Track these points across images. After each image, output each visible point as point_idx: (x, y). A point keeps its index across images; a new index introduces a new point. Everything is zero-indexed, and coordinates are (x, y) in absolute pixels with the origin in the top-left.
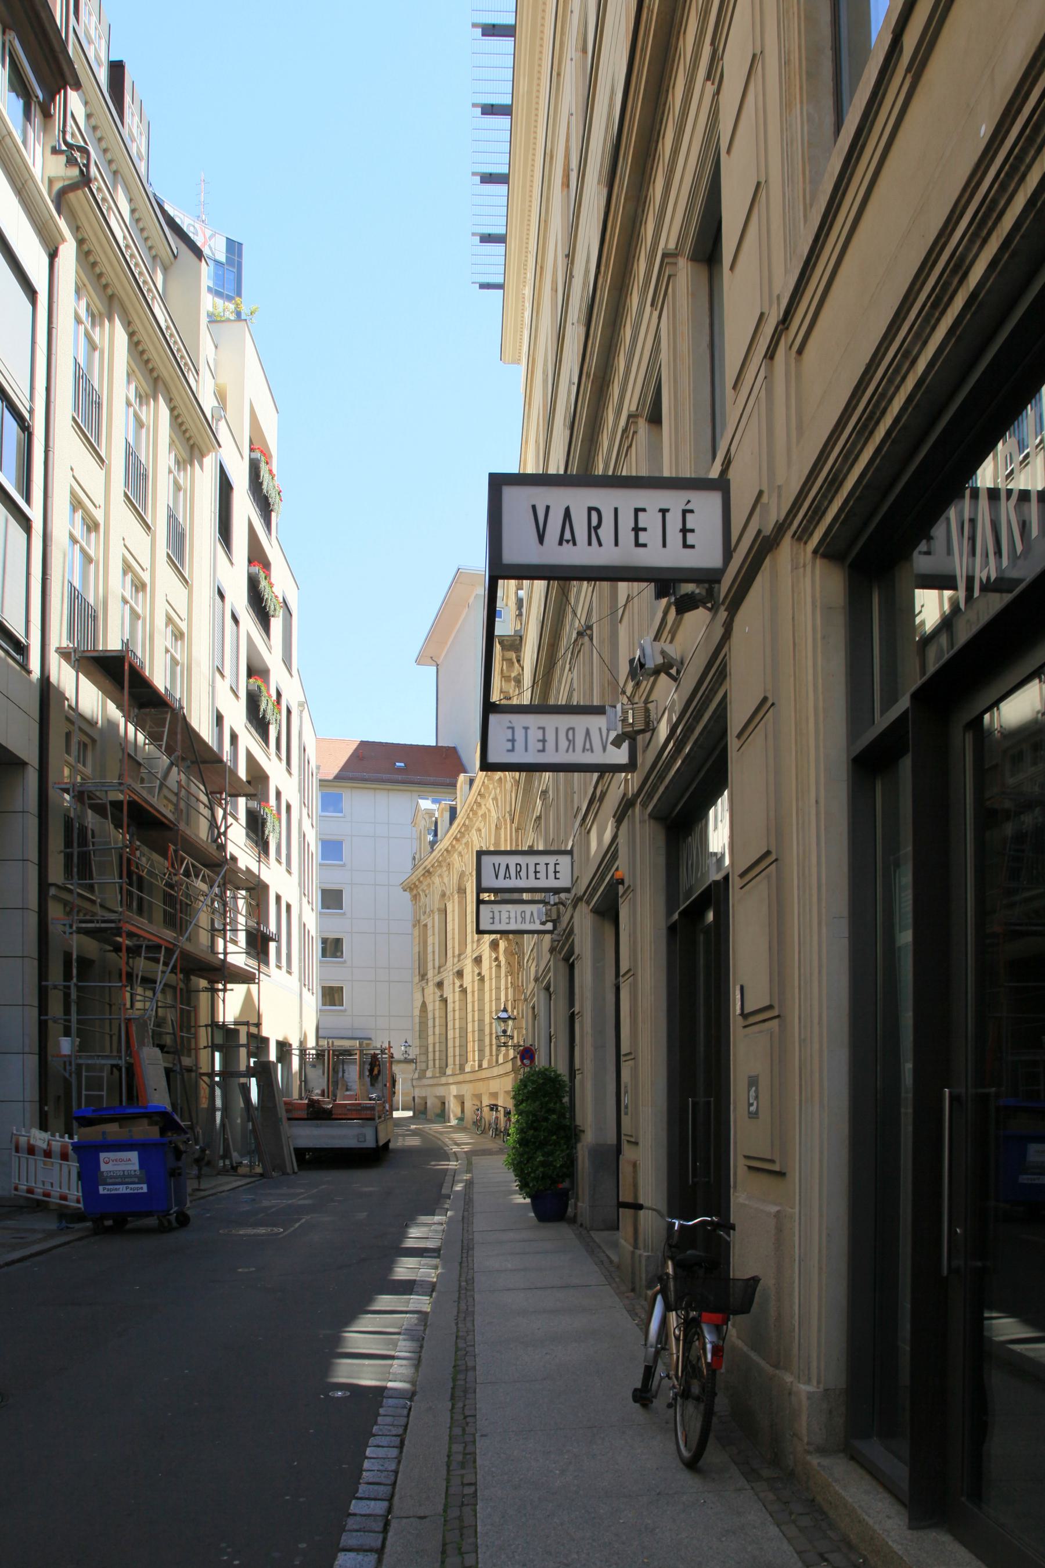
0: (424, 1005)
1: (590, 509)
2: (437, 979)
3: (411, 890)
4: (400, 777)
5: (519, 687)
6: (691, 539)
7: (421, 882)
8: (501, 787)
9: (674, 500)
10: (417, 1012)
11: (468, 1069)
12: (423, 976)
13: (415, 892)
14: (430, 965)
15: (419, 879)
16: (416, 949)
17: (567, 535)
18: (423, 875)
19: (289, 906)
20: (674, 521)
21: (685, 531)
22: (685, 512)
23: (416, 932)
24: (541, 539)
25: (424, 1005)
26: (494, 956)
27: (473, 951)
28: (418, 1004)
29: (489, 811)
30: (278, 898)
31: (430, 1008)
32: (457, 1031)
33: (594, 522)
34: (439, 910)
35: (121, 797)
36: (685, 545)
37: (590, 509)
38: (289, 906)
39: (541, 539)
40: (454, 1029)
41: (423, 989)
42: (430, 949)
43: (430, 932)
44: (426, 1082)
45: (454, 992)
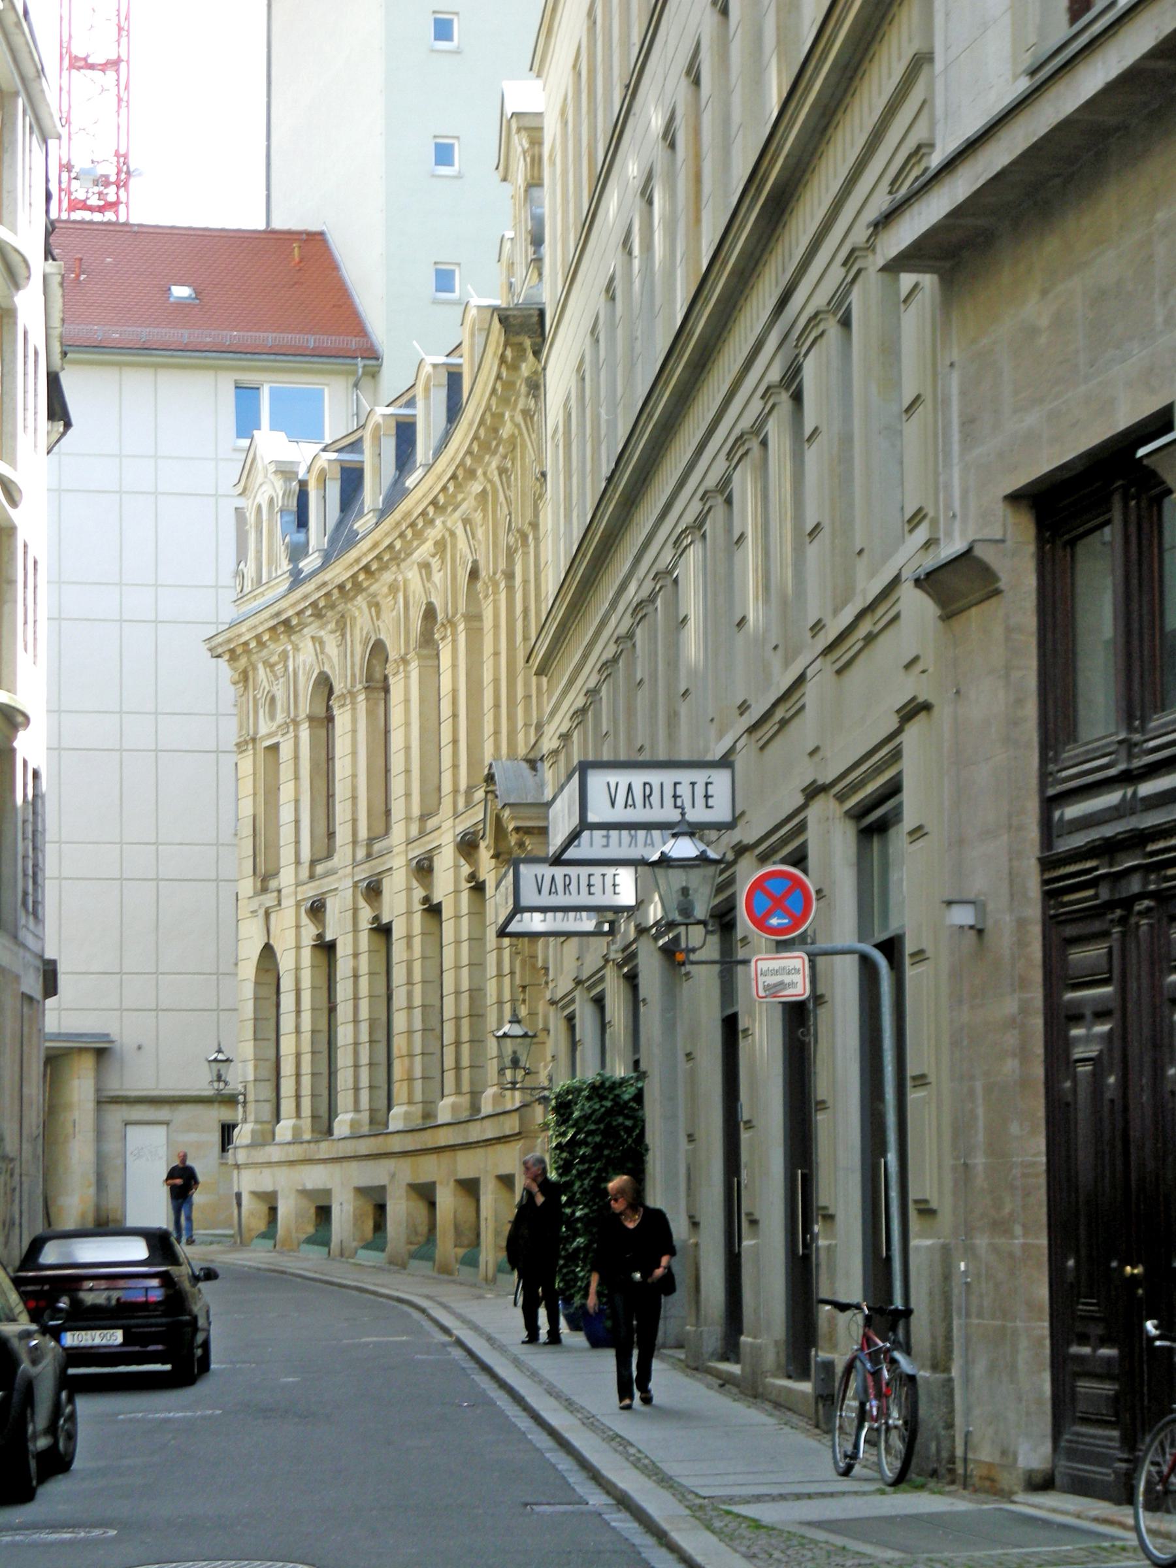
0: (268, 951)
1: (645, 784)
2: (310, 891)
3: (233, 656)
4: (184, 335)
5: (536, 397)
6: (711, 802)
7: (261, 644)
8: (484, 510)
9: (700, 776)
10: (248, 970)
11: (395, 1124)
12: (265, 879)
13: (243, 661)
14: (287, 855)
15: (258, 637)
16: (247, 808)
17: (630, 802)
18: (273, 629)
19: (36, 774)
20: (700, 791)
21: (707, 797)
22: (707, 784)
23: (246, 764)
24: (613, 804)
25: (268, 951)
26: (466, 870)
27: (409, 842)
28: (251, 951)
29: (453, 534)
30: (25, 763)
31: (286, 962)
32: (364, 1028)
33: (648, 793)
34: (311, 718)
35: (1146, 1520)
36: (707, 807)
37: (645, 784)
38: (36, 774)
39: (613, 804)
40: (356, 1021)
41: (267, 914)
42: (286, 814)
43: (286, 771)
44: (274, 1153)
45: (356, 930)
